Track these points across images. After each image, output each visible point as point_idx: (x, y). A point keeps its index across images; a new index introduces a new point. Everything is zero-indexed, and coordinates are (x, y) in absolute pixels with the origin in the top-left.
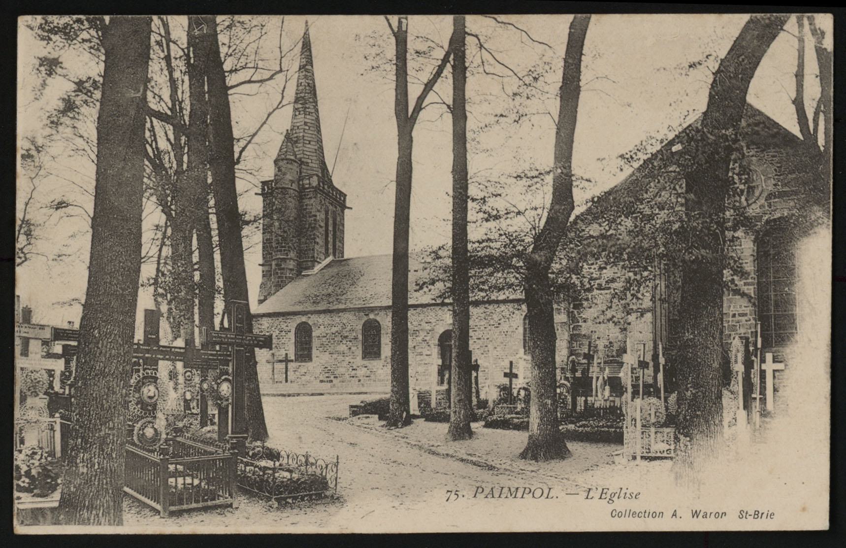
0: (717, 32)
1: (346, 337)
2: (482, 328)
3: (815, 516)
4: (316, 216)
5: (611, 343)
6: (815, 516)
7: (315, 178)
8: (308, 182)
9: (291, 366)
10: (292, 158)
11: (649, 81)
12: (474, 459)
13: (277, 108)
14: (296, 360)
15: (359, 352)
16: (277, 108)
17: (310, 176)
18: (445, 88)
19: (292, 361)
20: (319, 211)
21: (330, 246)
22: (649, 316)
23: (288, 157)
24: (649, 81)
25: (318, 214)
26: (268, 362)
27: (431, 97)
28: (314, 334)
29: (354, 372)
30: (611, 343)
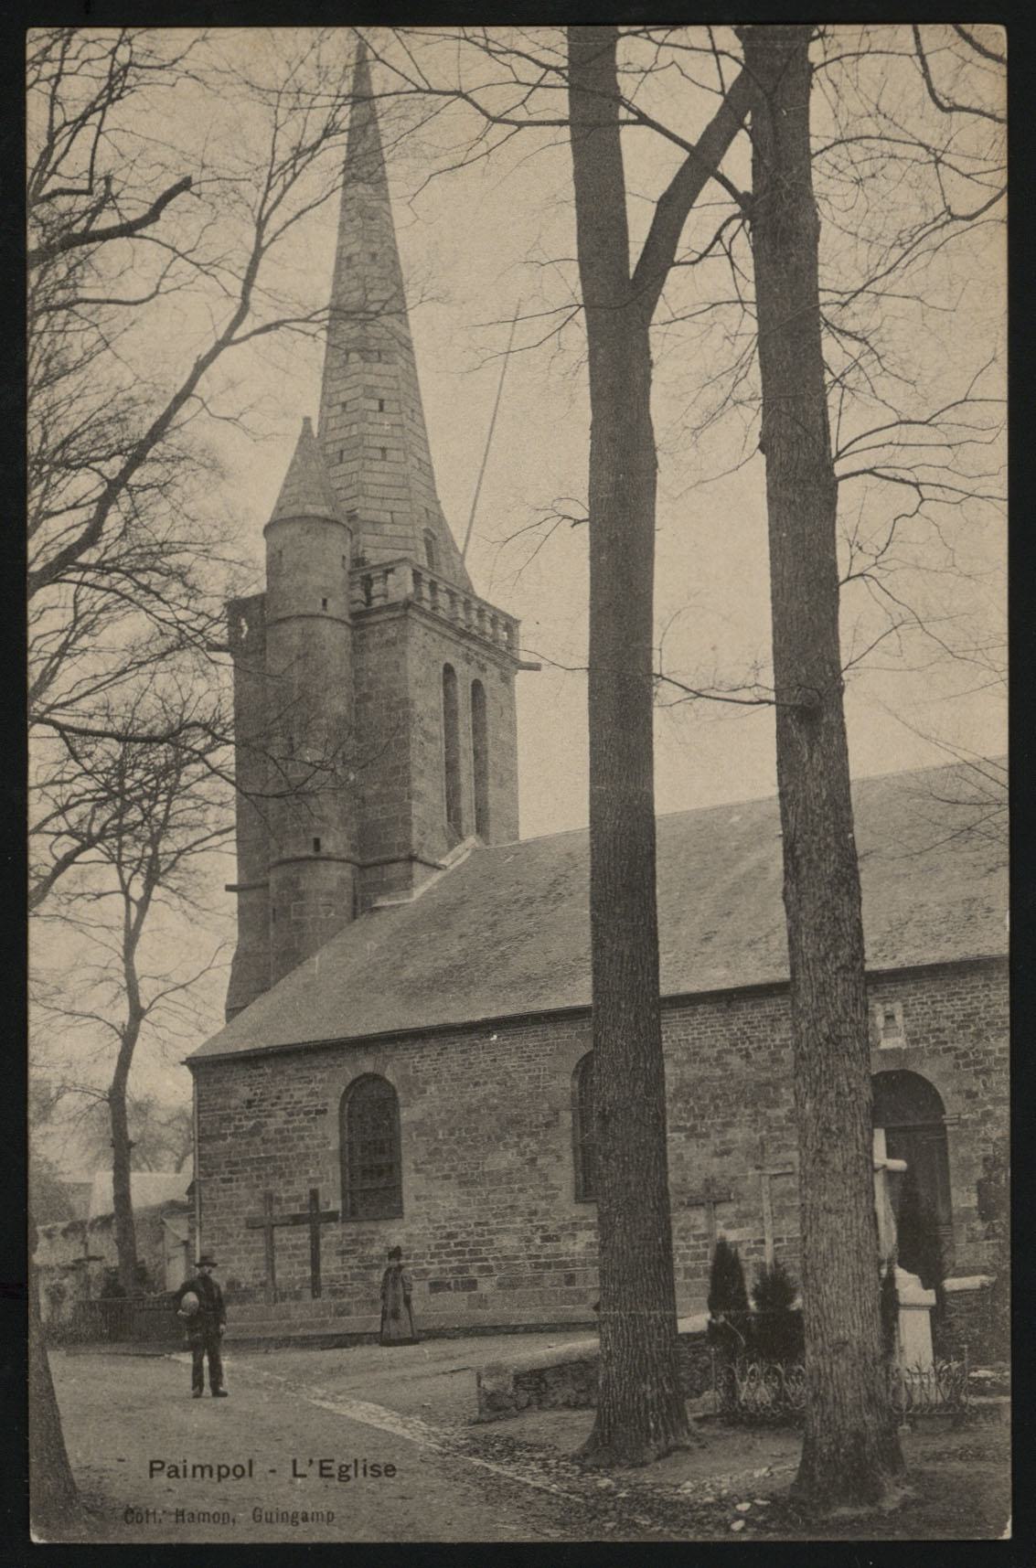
7: (406, 573)
9: (333, 1234)
10: (324, 511)
13: (225, 342)
14: (351, 1214)
16: (225, 342)
19: (333, 1217)
23: (310, 509)
28: (405, 1115)
29: (550, 1248)
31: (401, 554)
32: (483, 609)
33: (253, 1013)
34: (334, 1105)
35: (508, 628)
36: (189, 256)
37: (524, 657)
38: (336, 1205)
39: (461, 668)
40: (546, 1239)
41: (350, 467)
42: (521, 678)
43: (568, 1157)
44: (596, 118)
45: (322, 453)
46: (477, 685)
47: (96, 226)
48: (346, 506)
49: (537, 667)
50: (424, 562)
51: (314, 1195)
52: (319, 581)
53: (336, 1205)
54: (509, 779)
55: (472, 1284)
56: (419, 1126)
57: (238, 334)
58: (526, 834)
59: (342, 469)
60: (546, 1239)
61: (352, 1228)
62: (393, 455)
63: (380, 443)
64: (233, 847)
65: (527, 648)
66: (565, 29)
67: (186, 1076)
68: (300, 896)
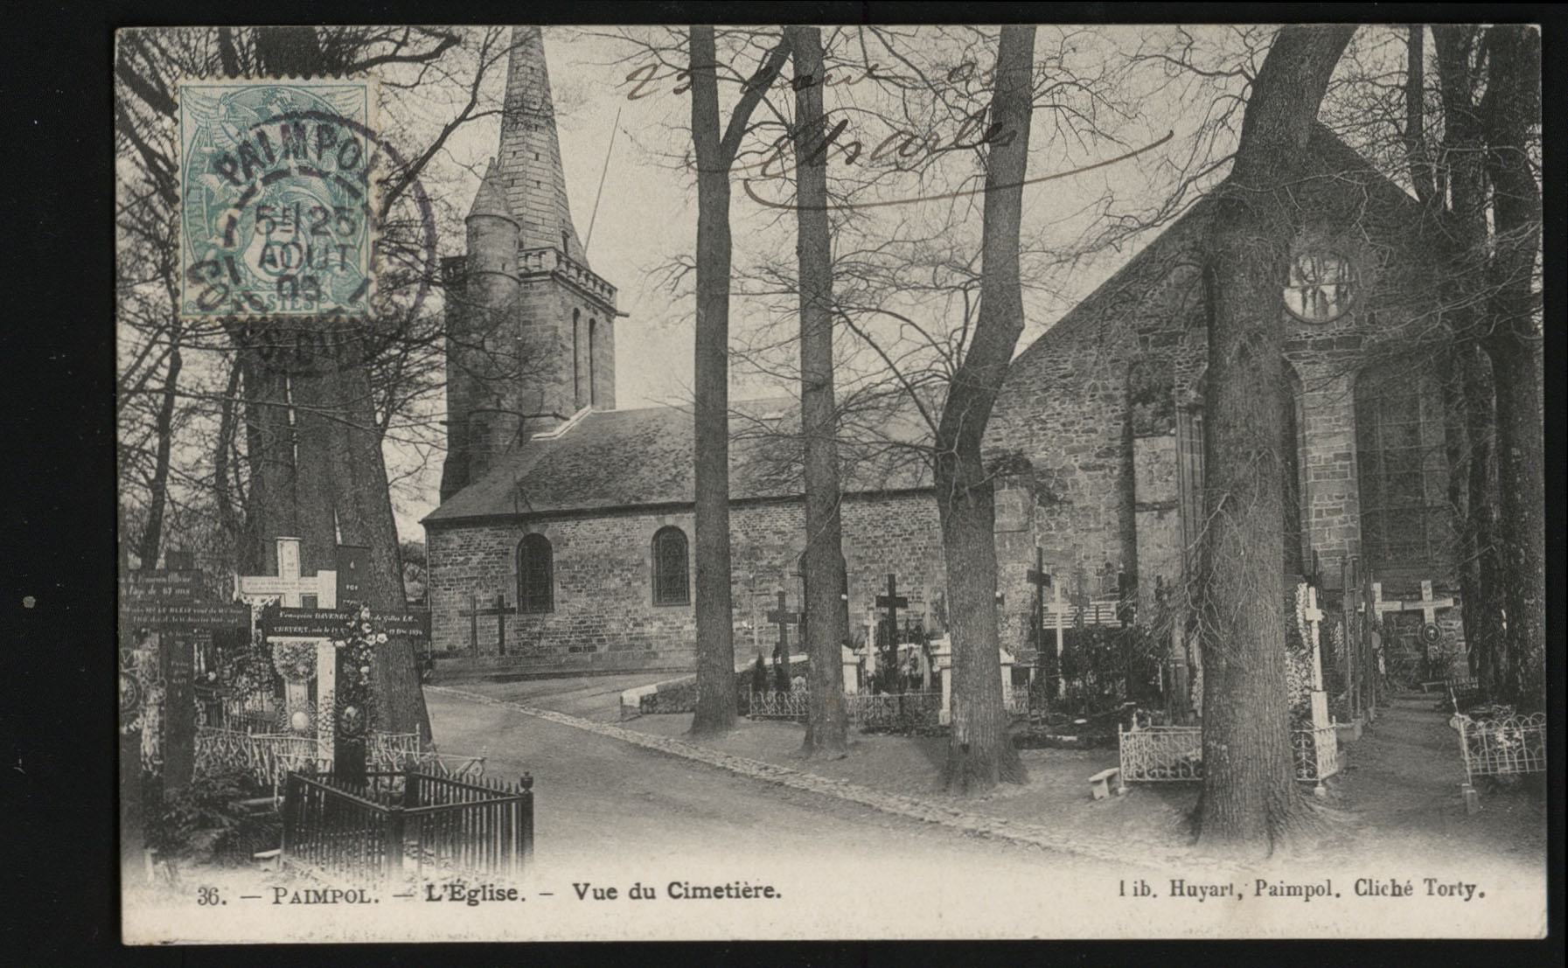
0: (1234, 48)
1: (621, 563)
2: (881, 542)
3: (1566, 6)
4: (556, 328)
5: (1108, 565)
6: (1566, 6)
7: (551, 255)
8: (536, 261)
9: (512, 622)
10: (503, 213)
11: (1139, 124)
12: (1172, 681)
13: (463, 118)
14: (522, 611)
15: (647, 592)
16: (463, 118)
17: (541, 252)
18: (783, 99)
19: (513, 610)
20: (560, 318)
21: (585, 386)
22: (1173, 517)
23: (494, 211)
24: (1139, 124)
25: (560, 324)
26: (462, 614)
27: (760, 112)
28: (555, 557)
29: (638, 629)
30: (1108, 565)
31: (548, 244)
32: (596, 279)
33: (458, 499)
34: (513, 550)
35: (610, 292)
36: (925, 340)
37: (619, 309)
38: (514, 605)
39: (583, 311)
40: (636, 625)
41: (517, 190)
42: (617, 320)
43: (649, 581)
44: (701, 75)
45: (498, 177)
46: (592, 322)
47: (399, 53)
48: (515, 211)
49: (627, 316)
50: (562, 249)
51: (501, 598)
52: (501, 253)
53: (514, 605)
54: (610, 375)
55: (593, 648)
56: (565, 564)
57: (470, 115)
58: (620, 407)
59: (513, 190)
60: (636, 625)
61: (524, 618)
62: (543, 186)
63: (537, 178)
64: (445, 396)
65: (620, 303)
66: (686, 29)
67: (422, 527)
68: (489, 431)
